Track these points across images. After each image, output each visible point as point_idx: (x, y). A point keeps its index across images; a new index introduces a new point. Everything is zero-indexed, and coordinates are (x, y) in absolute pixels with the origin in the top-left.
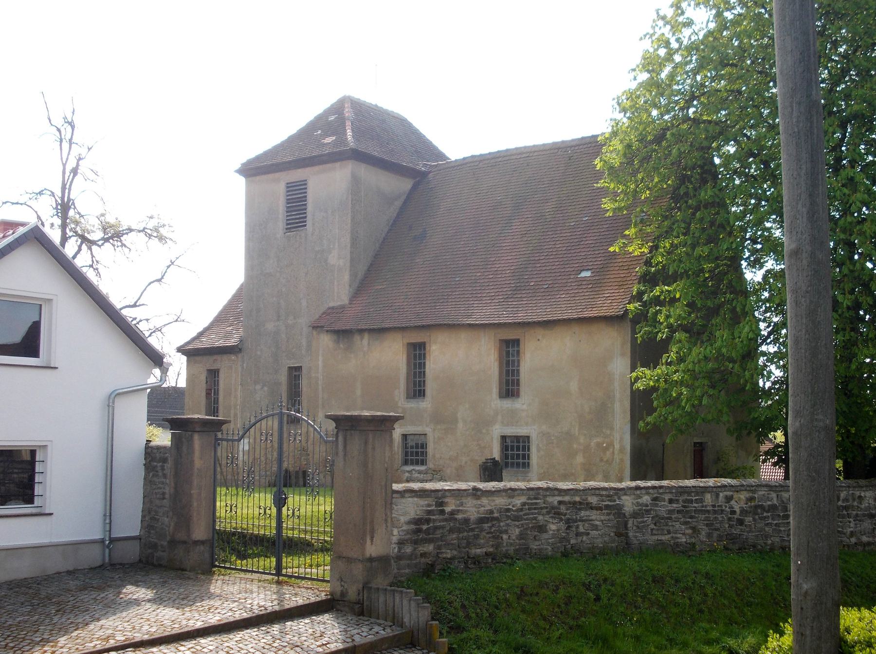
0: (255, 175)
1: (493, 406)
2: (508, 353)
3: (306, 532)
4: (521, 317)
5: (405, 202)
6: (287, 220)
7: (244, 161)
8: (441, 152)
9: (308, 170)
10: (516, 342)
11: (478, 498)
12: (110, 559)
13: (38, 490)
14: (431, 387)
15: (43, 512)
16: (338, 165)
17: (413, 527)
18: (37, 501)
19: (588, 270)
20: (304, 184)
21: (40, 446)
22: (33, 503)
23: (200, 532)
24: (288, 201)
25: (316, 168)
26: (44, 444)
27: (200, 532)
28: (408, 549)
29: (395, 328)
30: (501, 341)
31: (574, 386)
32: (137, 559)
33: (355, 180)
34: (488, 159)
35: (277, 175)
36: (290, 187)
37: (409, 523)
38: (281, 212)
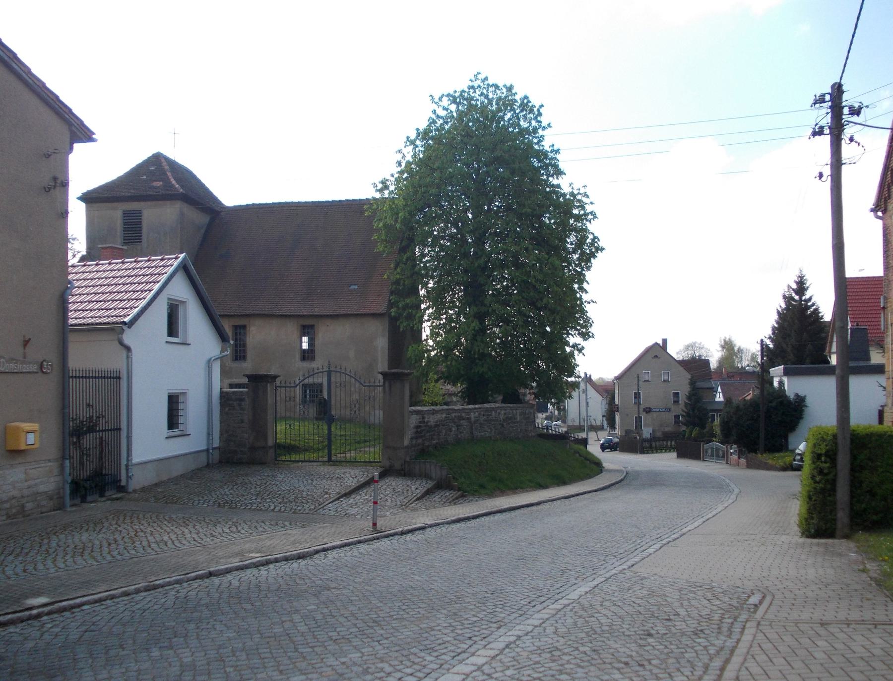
0: (92, 202)
1: (297, 366)
2: (236, 333)
3: (295, 440)
4: (317, 311)
5: (207, 231)
6: (125, 237)
7: (85, 191)
8: (833, 238)
9: (142, 204)
10: (244, 327)
11: (433, 414)
12: (212, 461)
13: (181, 420)
14: (250, 354)
15: (185, 433)
16: (168, 203)
17: (415, 430)
18: (181, 427)
19: (355, 285)
20: (139, 213)
21: (181, 393)
22: (178, 428)
23: (270, 442)
24: (125, 224)
25: (149, 203)
26: (185, 391)
27: (270, 442)
28: (414, 442)
29: (328, 315)
30: (233, 326)
31: (352, 354)
32: (206, 464)
33: (182, 214)
34: (266, 208)
35: (115, 205)
36: (126, 214)
37: (414, 428)
38: (118, 234)
